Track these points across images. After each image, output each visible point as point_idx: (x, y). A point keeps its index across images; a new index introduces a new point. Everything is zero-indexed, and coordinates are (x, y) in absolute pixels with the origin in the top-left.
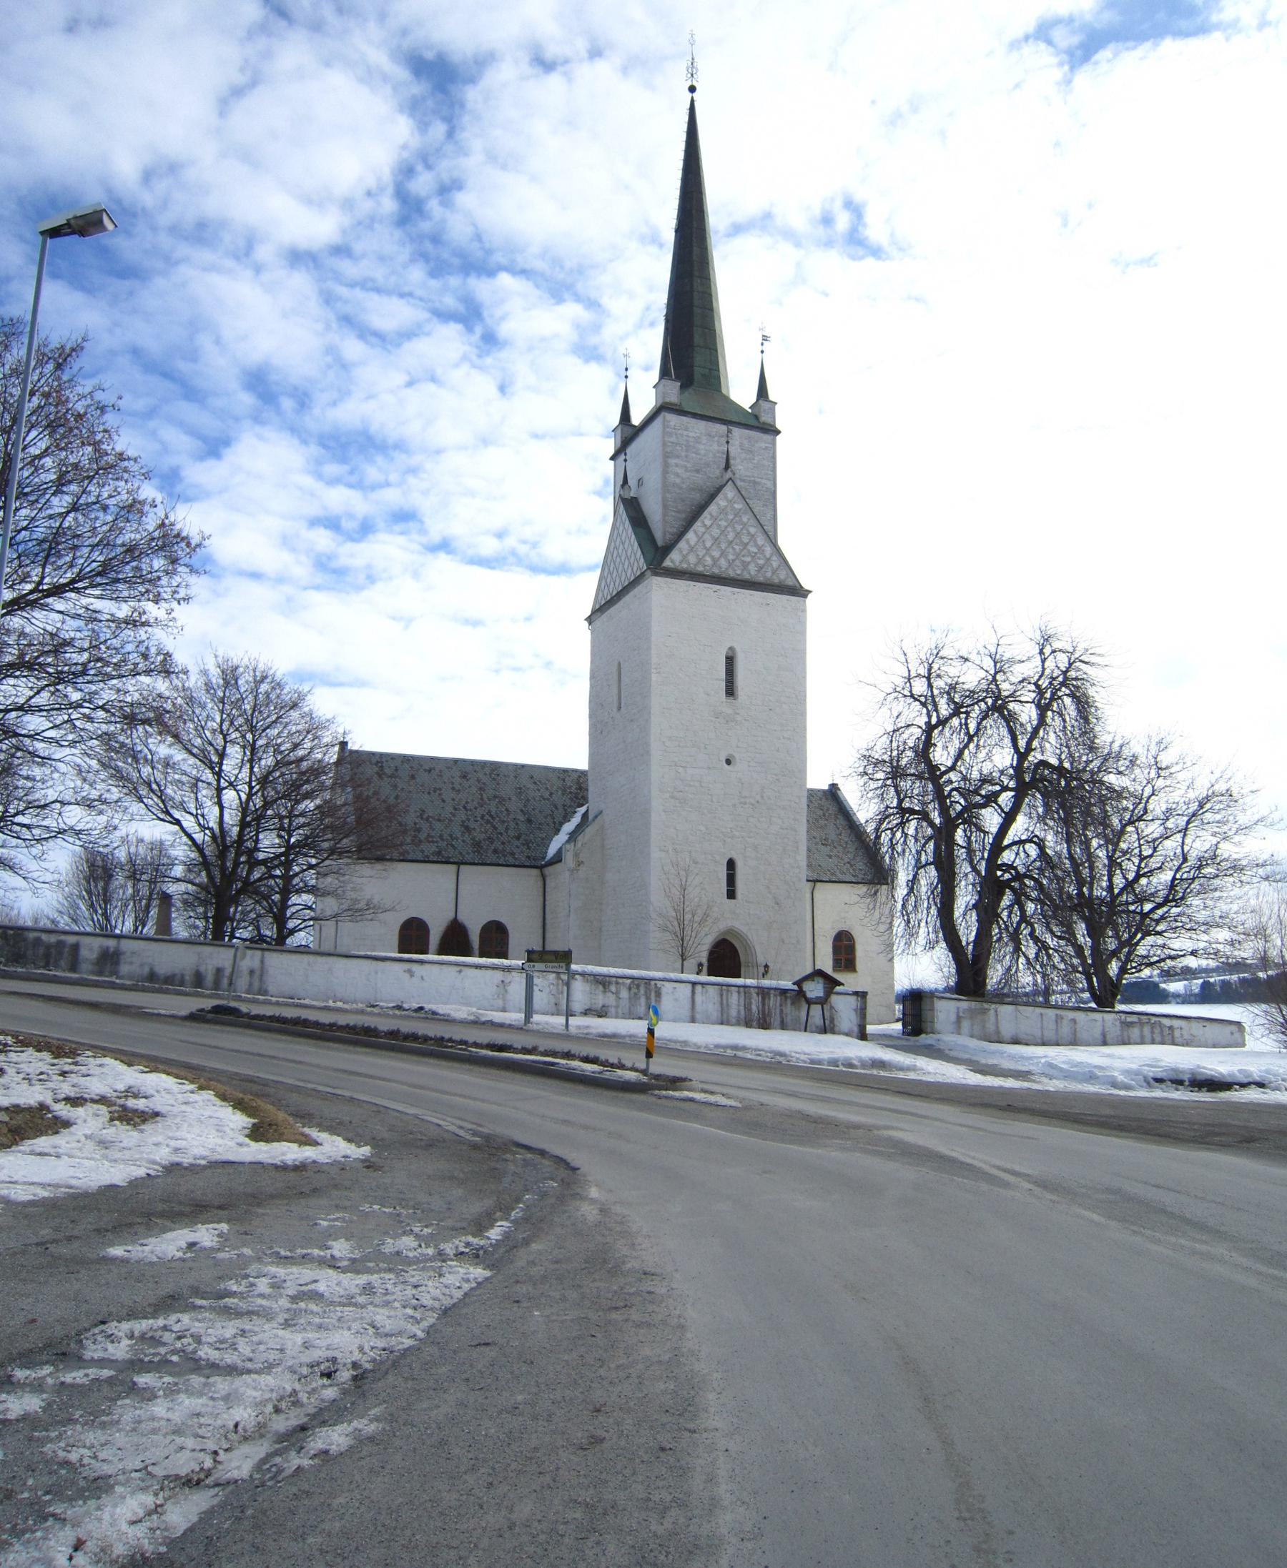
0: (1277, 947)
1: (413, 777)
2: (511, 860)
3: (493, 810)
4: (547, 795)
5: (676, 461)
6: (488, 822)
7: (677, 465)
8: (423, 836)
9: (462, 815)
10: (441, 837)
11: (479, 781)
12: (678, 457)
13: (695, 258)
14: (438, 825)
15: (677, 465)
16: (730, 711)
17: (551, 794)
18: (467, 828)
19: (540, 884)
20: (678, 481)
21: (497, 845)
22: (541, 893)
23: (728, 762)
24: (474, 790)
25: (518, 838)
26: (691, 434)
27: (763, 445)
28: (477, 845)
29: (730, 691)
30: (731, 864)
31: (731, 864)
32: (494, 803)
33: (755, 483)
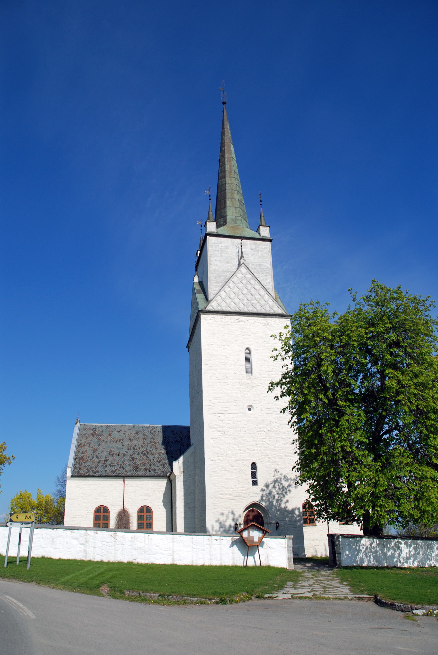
0: (1, 579)
1: (110, 435)
2: (153, 473)
3: (148, 448)
4: (179, 439)
5: (216, 258)
6: (145, 454)
7: (216, 260)
8: (108, 463)
9: (131, 452)
10: (118, 463)
11: (144, 435)
12: (216, 256)
13: (226, 169)
14: (117, 458)
15: (216, 260)
16: (249, 381)
17: (182, 439)
18: (133, 458)
19: (170, 484)
20: (217, 268)
21: (148, 466)
22: (170, 488)
23: (250, 409)
24: (141, 439)
25: (159, 462)
26: (223, 245)
27: (264, 247)
28: (136, 468)
29: (249, 370)
30: (254, 465)
31: (254, 465)
32: (149, 445)
33: (259, 265)
